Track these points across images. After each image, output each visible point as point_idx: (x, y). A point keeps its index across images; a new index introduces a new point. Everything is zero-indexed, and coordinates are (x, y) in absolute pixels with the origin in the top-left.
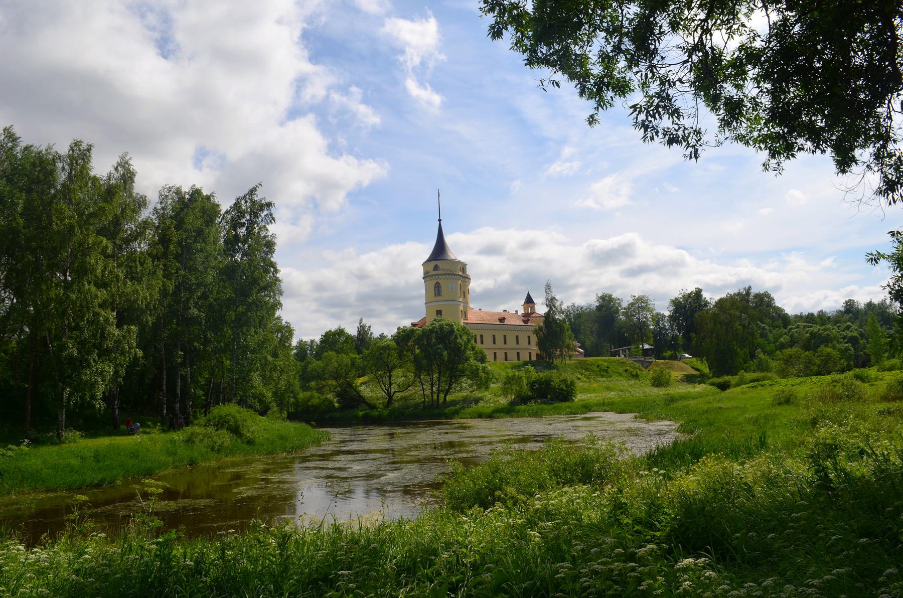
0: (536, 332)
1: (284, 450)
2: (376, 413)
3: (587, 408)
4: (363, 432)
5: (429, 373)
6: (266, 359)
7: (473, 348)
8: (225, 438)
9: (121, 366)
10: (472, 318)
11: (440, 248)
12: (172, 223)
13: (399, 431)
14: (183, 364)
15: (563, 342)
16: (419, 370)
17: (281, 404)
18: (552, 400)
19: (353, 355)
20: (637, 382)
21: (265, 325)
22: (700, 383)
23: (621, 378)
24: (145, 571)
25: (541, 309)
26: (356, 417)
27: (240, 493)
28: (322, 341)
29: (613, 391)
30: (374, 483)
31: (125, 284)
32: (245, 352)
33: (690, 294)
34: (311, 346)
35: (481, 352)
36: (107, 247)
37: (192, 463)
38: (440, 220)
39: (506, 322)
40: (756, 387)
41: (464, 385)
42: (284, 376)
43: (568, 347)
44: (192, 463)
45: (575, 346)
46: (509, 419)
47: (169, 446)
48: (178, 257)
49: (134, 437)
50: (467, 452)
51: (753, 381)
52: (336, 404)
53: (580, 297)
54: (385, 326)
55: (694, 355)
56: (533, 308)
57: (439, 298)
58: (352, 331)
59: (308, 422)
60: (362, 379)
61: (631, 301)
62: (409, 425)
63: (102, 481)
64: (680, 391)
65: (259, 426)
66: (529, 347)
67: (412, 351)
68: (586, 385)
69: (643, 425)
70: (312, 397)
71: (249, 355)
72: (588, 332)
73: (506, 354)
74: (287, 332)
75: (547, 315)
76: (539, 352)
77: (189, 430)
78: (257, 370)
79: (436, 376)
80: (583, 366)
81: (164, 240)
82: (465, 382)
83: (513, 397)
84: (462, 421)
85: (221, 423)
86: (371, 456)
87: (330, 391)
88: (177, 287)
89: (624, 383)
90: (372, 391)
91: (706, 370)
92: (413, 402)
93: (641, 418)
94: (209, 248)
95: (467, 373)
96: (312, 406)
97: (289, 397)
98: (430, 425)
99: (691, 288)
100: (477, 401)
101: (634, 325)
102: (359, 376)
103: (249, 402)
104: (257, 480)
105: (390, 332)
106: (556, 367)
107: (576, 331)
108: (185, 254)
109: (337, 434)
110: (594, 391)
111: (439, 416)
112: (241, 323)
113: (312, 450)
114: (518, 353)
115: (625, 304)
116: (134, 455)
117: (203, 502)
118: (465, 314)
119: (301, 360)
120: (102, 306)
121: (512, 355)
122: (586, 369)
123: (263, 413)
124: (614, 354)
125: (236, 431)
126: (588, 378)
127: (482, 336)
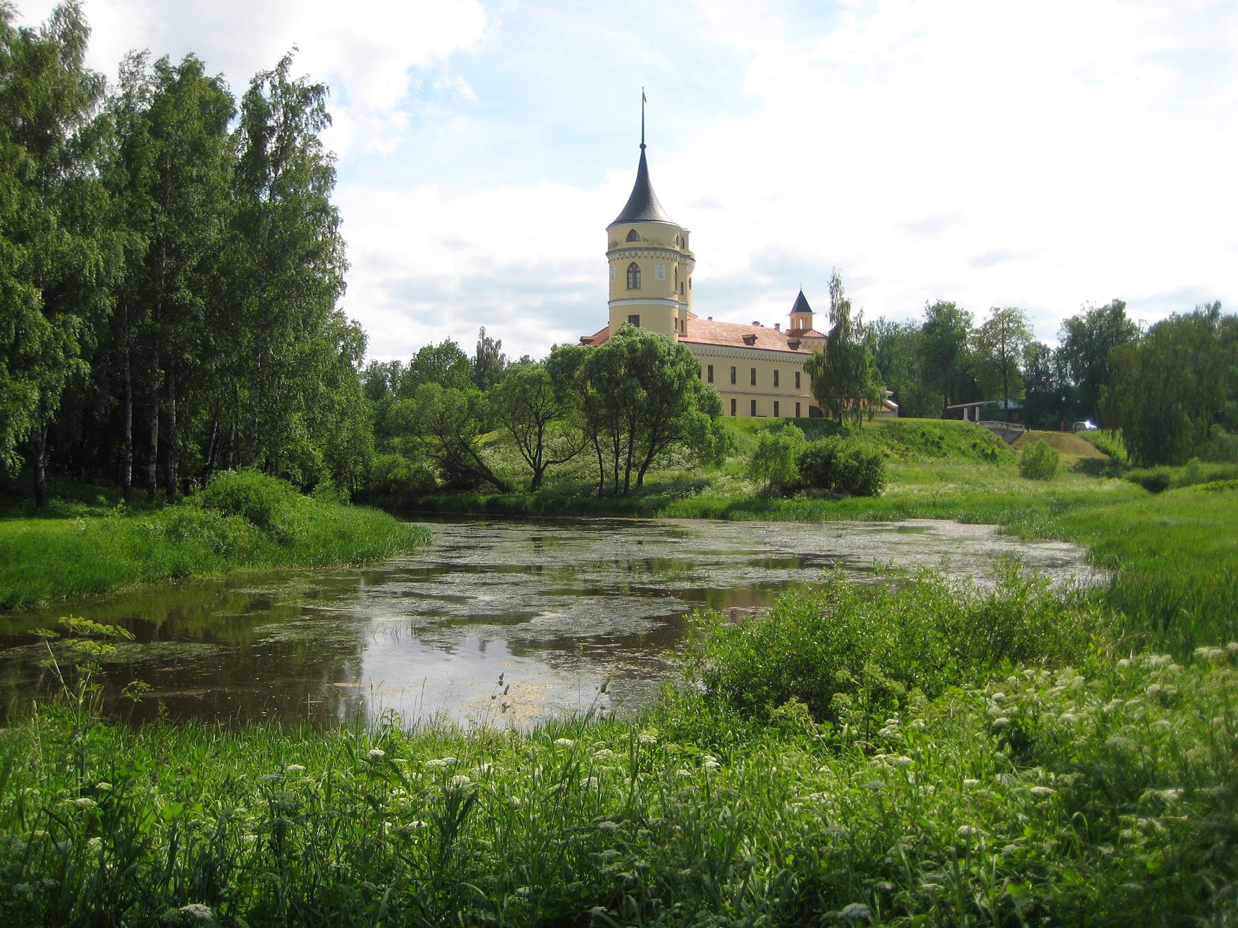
0: (810, 367)
1: (346, 557)
2: (511, 499)
3: (903, 510)
4: (489, 533)
5: (614, 432)
6: (315, 389)
7: (697, 390)
8: (239, 529)
9: (54, 389)
10: (695, 334)
11: (641, 198)
12: (144, 124)
13: (549, 533)
14: (164, 392)
15: (862, 386)
16: (594, 426)
17: (339, 475)
18: (839, 491)
19: (474, 392)
20: (994, 467)
21: (315, 326)
22: (1110, 476)
23: (964, 459)
24: (53, 890)
25: (822, 325)
26: (475, 506)
27: (268, 635)
28: (415, 365)
29: (952, 481)
30: (518, 629)
31: (60, 238)
32: (275, 374)
33: (1100, 313)
34: (394, 374)
35: (711, 398)
36: (25, 165)
37: (178, 573)
38: (643, 147)
39: (757, 344)
40: (1221, 489)
41: (675, 457)
42: (347, 423)
43: (870, 397)
44: (178, 573)
45: (883, 396)
46: (759, 524)
47: (138, 540)
48: (155, 191)
49: (74, 522)
50: (691, 579)
51: (1213, 478)
52: (438, 480)
53: (891, 301)
54: (529, 341)
55: (1101, 425)
56: (808, 321)
57: (635, 293)
58: (471, 352)
59: (388, 509)
60: (486, 438)
61: (990, 317)
62: (573, 523)
63: (13, 598)
64: (1076, 489)
65: (302, 513)
66: (796, 392)
67: (582, 389)
68: (901, 468)
69: (1019, 548)
70: (395, 464)
71: (283, 380)
72: (906, 372)
73: (753, 403)
74: (357, 340)
75: (835, 333)
76: (816, 403)
77: (174, 512)
78: (298, 409)
79: (624, 437)
80: (895, 433)
81: (130, 154)
82: (679, 451)
83: (768, 482)
84: (673, 521)
85: (233, 503)
86: (510, 577)
87: (428, 455)
88: (155, 249)
89: (969, 469)
90: (505, 460)
91: (1122, 454)
92: (579, 483)
93: (1010, 533)
94: (213, 175)
95: (684, 433)
96: (395, 481)
97: (356, 463)
98: (613, 526)
99: (1103, 301)
100: (700, 486)
101: (993, 363)
102: (482, 432)
103: (282, 467)
104: (295, 612)
105: (540, 354)
106: (845, 434)
107: (885, 369)
108: (168, 187)
109: (441, 534)
110: (916, 479)
111: (628, 510)
112: (267, 320)
113: (399, 560)
114: (776, 404)
115: (978, 323)
116: (73, 553)
117: (198, 649)
118: (682, 325)
119: (376, 398)
120: (21, 275)
121: (765, 406)
122: (901, 440)
123: (307, 490)
124: (948, 415)
125: (260, 518)
126: (902, 455)
127: (711, 368)
